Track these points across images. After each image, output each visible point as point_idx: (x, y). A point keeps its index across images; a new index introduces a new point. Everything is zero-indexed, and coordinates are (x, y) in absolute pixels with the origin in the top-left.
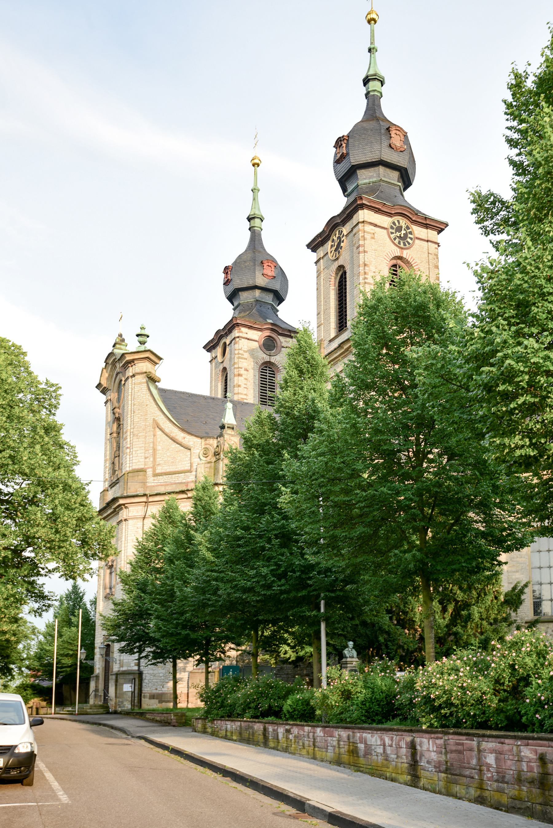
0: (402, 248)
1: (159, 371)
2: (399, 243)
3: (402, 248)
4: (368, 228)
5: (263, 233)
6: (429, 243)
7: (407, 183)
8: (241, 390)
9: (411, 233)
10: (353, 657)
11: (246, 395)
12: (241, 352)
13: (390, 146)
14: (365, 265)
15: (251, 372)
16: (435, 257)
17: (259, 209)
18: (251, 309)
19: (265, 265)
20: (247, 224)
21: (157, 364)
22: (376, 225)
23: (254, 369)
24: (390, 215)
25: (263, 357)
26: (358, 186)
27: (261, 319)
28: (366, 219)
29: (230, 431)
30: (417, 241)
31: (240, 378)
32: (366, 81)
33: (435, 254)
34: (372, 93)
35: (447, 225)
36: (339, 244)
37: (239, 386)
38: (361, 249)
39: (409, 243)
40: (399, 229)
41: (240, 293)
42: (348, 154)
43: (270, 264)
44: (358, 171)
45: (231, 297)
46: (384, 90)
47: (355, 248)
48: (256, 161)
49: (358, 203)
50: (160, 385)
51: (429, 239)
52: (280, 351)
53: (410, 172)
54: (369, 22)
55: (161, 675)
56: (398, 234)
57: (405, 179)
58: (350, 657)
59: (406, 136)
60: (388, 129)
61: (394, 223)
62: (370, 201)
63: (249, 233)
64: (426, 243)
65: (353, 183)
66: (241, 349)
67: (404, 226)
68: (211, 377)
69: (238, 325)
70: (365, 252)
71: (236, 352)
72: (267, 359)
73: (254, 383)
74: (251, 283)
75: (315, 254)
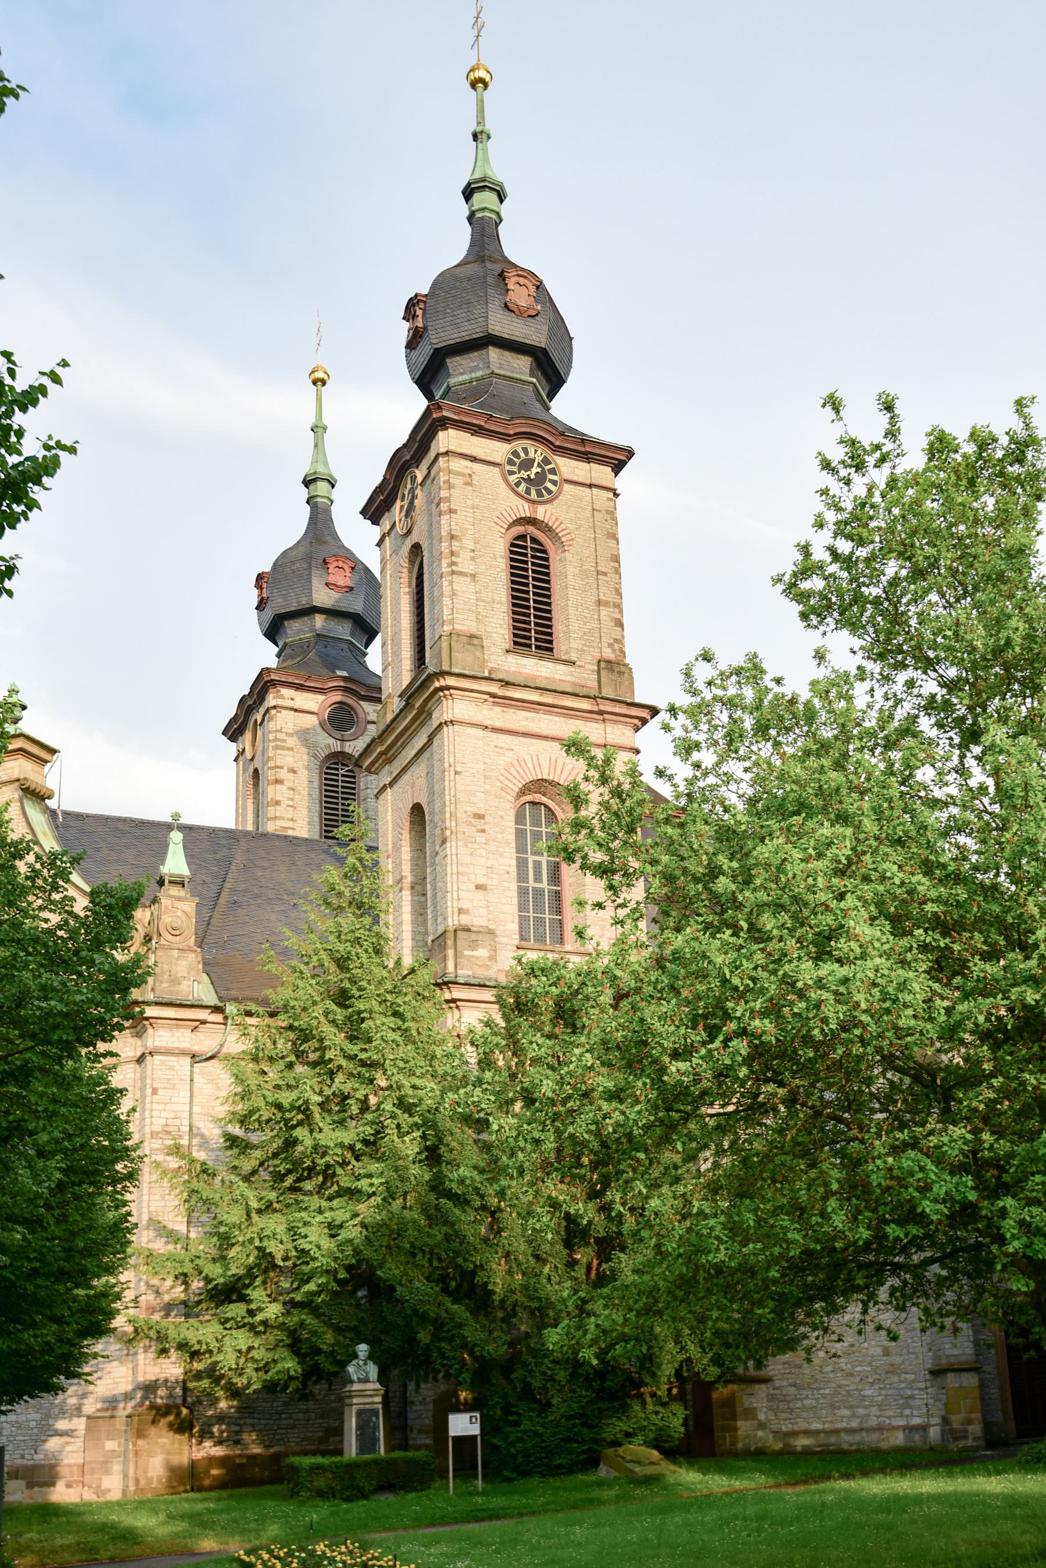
0: (534, 502)
1: (51, 777)
2: (528, 491)
3: (534, 502)
4: (459, 465)
5: (334, 509)
6: (595, 490)
7: (555, 380)
8: (279, 811)
9: (553, 471)
10: (366, 1380)
11: (292, 820)
12: (280, 736)
13: (506, 306)
14: (452, 537)
15: (303, 775)
16: (608, 517)
17: (326, 463)
18: (305, 653)
19: (331, 567)
20: (304, 493)
21: (46, 762)
22: (474, 459)
23: (308, 768)
24: (505, 438)
25: (328, 743)
26: (449, 388)
27: (324, 671)
28: (452, 448)
29: (175, 891)
30: (567, 487)
31: (279, 787)
32: (468, 193)
33: (607, 512)
34: (479, 215)
35: (630, 453)
36: (411, 503)
37: (277, 803)
38: (444, 507)
39: (549, 492)
40: (527, 464)
41: (286, 623)
42: (425, 328)
43: (340, 564)
44: (448, 361)
45: (272, 632)
46: (505, 209)
47: (434, 506)
48: (320, 375)
49: (435, 416)
50: (51, 803)
51: (594, 482)
52: (365, 729)
53: (555, 356)
54: (473, 85)
55: (33, 1424)
56: (524, 474)
57: (549, 371)
58: (360, 1381)
59: (540, 286)
60: (502, 276)
61: (515, 454)
62: (459, 411)
63: (307, 509)
64: (588, 490)
65: (442, 385)
66: (280, 731)
67: (539, 459)
68: (237, 791)
69: (273, 683)
70: (451, 511)
71: (271, 737)
72: (337, 746)
73: (310, 795)
74: (304, 602)
75: (377, 528)
